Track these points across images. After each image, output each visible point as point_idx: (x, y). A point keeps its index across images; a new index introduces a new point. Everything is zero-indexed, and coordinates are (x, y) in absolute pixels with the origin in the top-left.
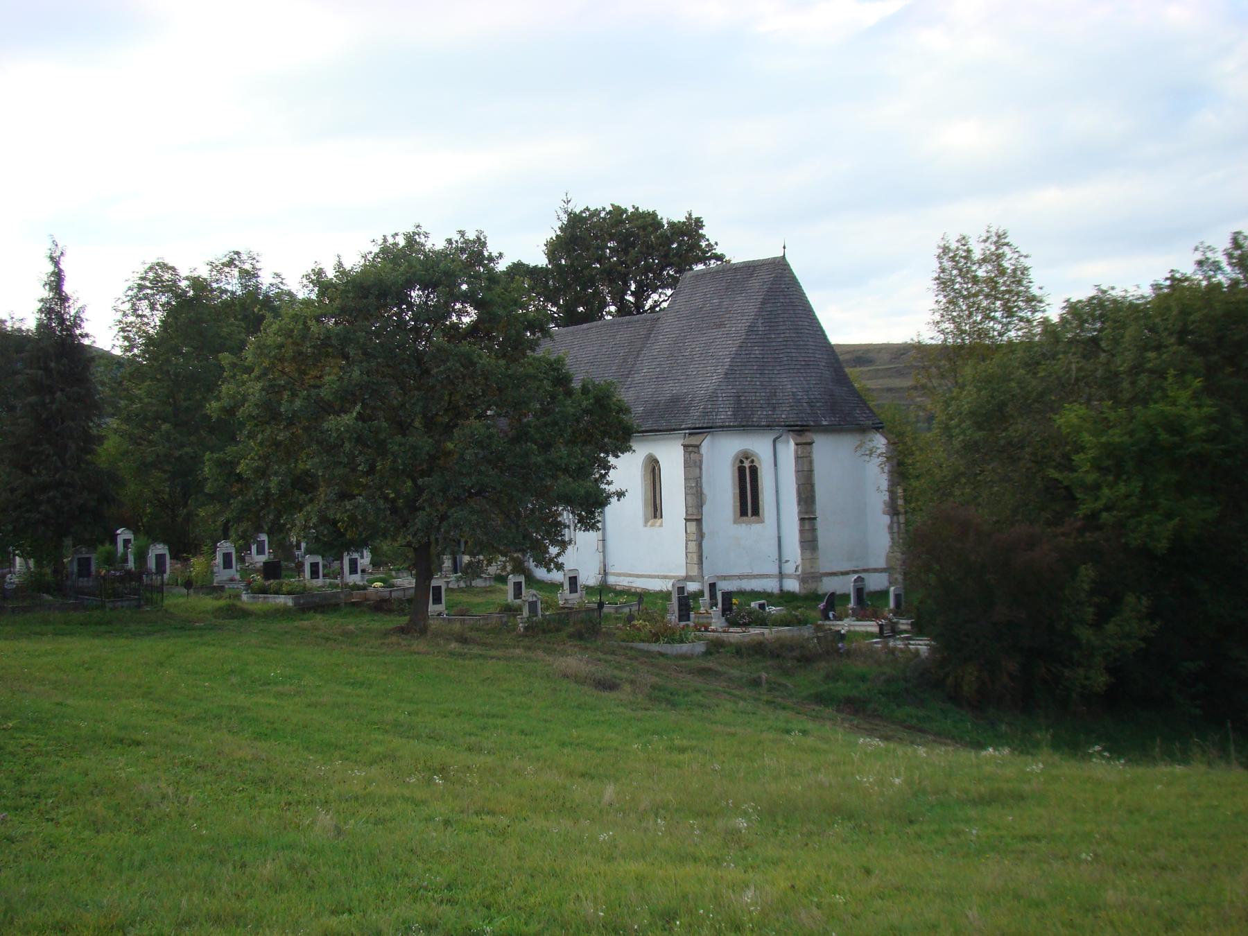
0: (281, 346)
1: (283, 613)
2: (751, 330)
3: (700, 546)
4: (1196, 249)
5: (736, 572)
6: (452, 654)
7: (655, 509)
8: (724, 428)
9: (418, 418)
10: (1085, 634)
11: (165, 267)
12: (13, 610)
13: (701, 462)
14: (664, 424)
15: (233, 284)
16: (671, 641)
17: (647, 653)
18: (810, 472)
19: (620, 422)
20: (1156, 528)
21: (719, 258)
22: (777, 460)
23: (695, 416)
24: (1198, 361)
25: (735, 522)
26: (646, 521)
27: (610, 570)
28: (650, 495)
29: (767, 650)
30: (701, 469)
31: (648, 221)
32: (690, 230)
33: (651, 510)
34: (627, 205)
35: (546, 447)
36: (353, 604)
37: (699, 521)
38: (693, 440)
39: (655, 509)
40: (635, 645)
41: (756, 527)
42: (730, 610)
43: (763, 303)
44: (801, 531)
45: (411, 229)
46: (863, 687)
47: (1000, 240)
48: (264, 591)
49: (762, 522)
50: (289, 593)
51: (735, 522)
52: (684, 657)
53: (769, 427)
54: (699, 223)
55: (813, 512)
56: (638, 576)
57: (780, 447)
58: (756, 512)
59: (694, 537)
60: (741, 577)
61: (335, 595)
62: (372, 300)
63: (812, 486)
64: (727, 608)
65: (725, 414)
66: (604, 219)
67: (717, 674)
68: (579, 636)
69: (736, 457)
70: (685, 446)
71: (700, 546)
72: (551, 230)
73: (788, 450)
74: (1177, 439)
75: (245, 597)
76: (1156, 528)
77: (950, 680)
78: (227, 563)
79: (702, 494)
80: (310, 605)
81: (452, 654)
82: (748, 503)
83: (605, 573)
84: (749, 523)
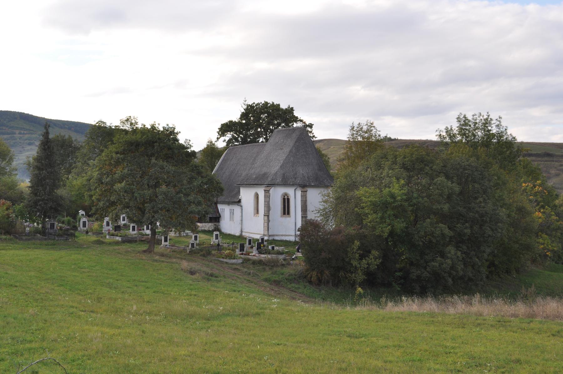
0: (105, 161)
1: (117, 243)
3: (268, 224)
6: (156, 261)
7: (257, 211)
10: (355, 263)
11: (101, 122)
12: (26, 239)
13: (270, 196)
14: (260, 182)
15: (127, 127)
16: (231, 258)
20: (384, 229)
21: (301, 121)
22: (295, 196)
24: (405, 174)
27: (243, 231)
28: (256, 206)
29: (261, 262)
32: (290, 111)
33: (256, 211)
34: (270, 101)
35: (187, 195)
36: (142, 241)
37: (268, 216)
38: (268, 189)
39: (257, 211)
41: (288, 219)
44: (302, 221)
45: (153, 123)
46: (281, 276)
48: (113, 235)
50: (120, 236)
52: (233, 264)
53: (293, 185)
54: (292, 109)
57: (297, 192)
58: (288, 213)
60: (282, 235)
61: (136, 238)
63: (306, 206)
64: (259, 248)
65: (279, 180)
67: (239, 270)
68: (204, 255)
70: (265, 191)
71: (268, 224)
73: (299, 193)
74: (392, 200)
75: (107, 237)
76: (384, 229)
77: (309, 276)
78: (108, 224)
80: (128, 240)
81: (156, 261)
82: (286, 211)
83: (242, 232)
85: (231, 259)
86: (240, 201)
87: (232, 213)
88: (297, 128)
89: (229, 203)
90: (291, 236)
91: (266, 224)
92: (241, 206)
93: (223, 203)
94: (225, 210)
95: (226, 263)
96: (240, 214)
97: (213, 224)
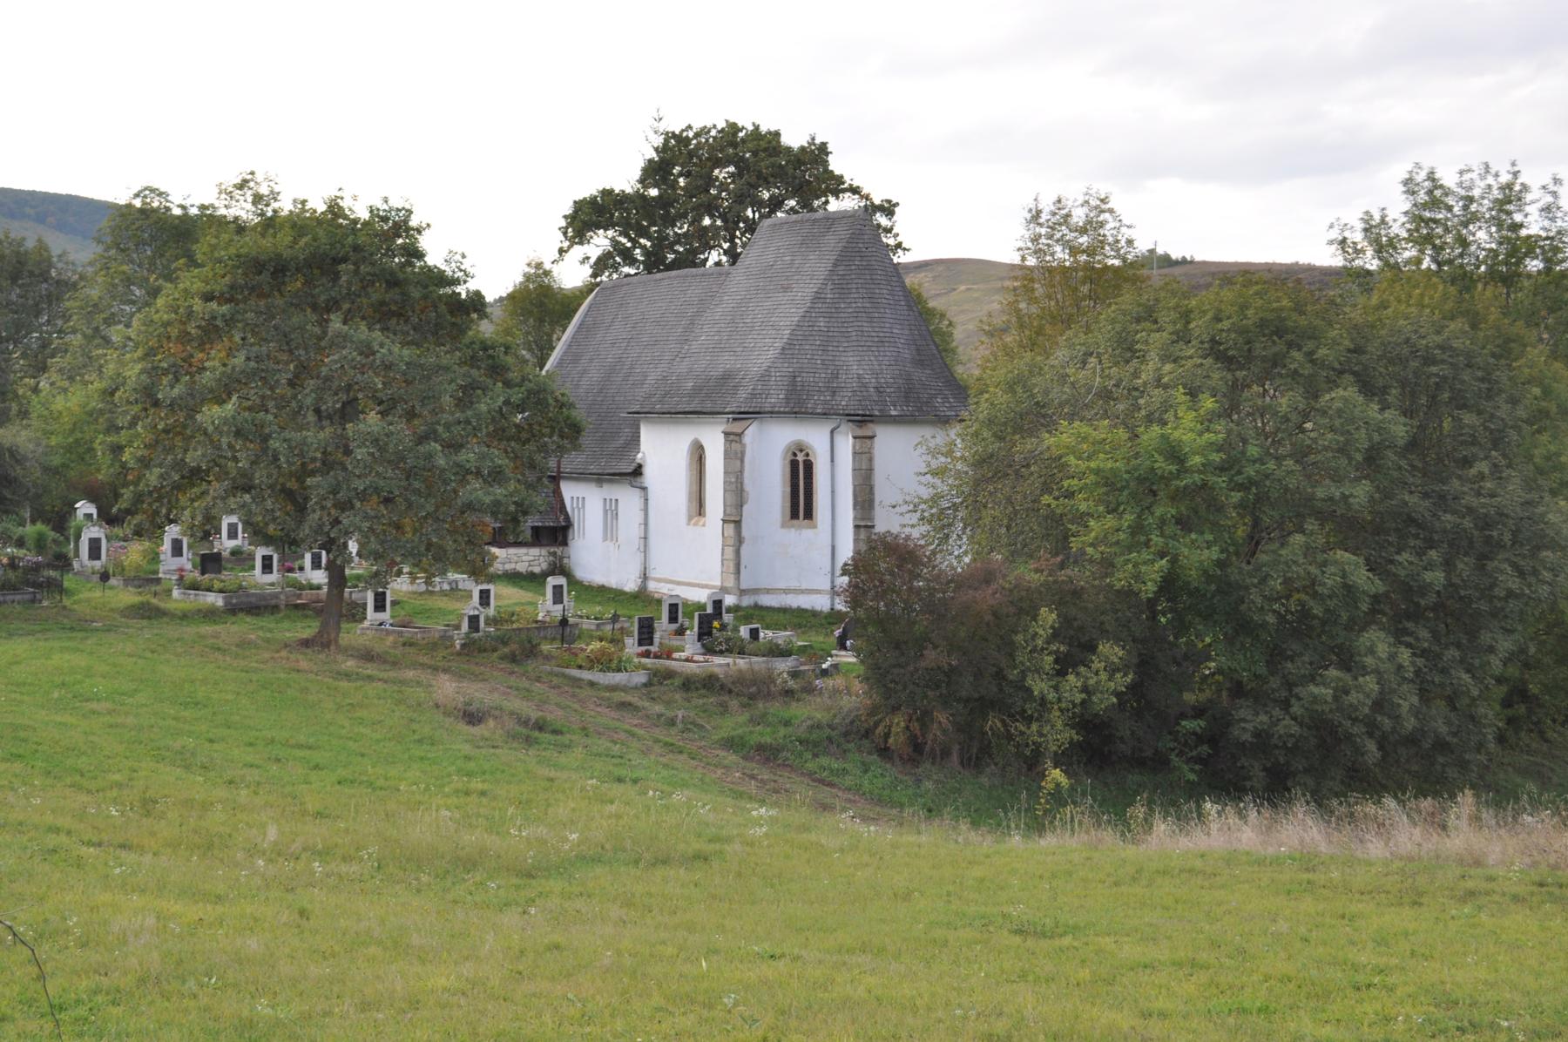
1: (209, 614)
2: (818, 297)
3: (738, 553)
4: (1331, 226)
5: (782, 585)
6: (347, 676)
7: (698, 505)
8: (774, 414)
9: (316, 405)
10: (1039, 686)
13: (743, 453)
14: (708, 406)
15: (243, 210)
17: (577, 682)
18: (869, 471)
19: (568, 418)
20: (1143, 568)
23: (740, 400)
25: (783, 526)
26: (690, 518)
27: (652, 574)
28: (695, 488)
30: (742, 461)
31: (767, 143)
32: (817, 154)
33: (695, 504)
34: (746, 122)
36: (296, 606)
37: (738, 523)
38: (736, 427)
39: (698, 505)
40: (567, 671)
41: (807, 533)
42: (710, 634)
43: (835, 265)
45: (334, 193)
46: (782, 731)
47: (1102, 205)
48: (195, 586)
49: (815, 527)
50: (221, 591)
51: (783, 526)
53: (825, 415)
54: (823, 149)
55: (871, 519)
56: (679, 583)
57: (839, 439)
58: (809, 514)
59: (731, 542)
60: (786, 591)
61: (276, 596)
62: (265, 277)
65: (776, 398)
66: (715, 138)
67: (637, 708)
68: (513, 659)
69: (788, 449)
70: (726, 434)
71: (738, 553)
72: (645, 150)
73: (846, 445)
74: (1173, 468)
75: (176, 593)
76: (1143, 568)
77: (880, 730)
78: (177, 549)
79: (742, 490)
81: (347, 676)
82: (801, 504)
83: (645, 577)
84: (800, 527)
85: (609, 669)
86: (638, 471)
87: (611, 512)
88: (842, 216)
89: (600, 478)
90: (818, 592)
91: (730, 551)
92: (644, 489)
93: (581, 477)
94: (585, 502)
95: (592, 684)
96: (640, 518)
97: (544, 551)
